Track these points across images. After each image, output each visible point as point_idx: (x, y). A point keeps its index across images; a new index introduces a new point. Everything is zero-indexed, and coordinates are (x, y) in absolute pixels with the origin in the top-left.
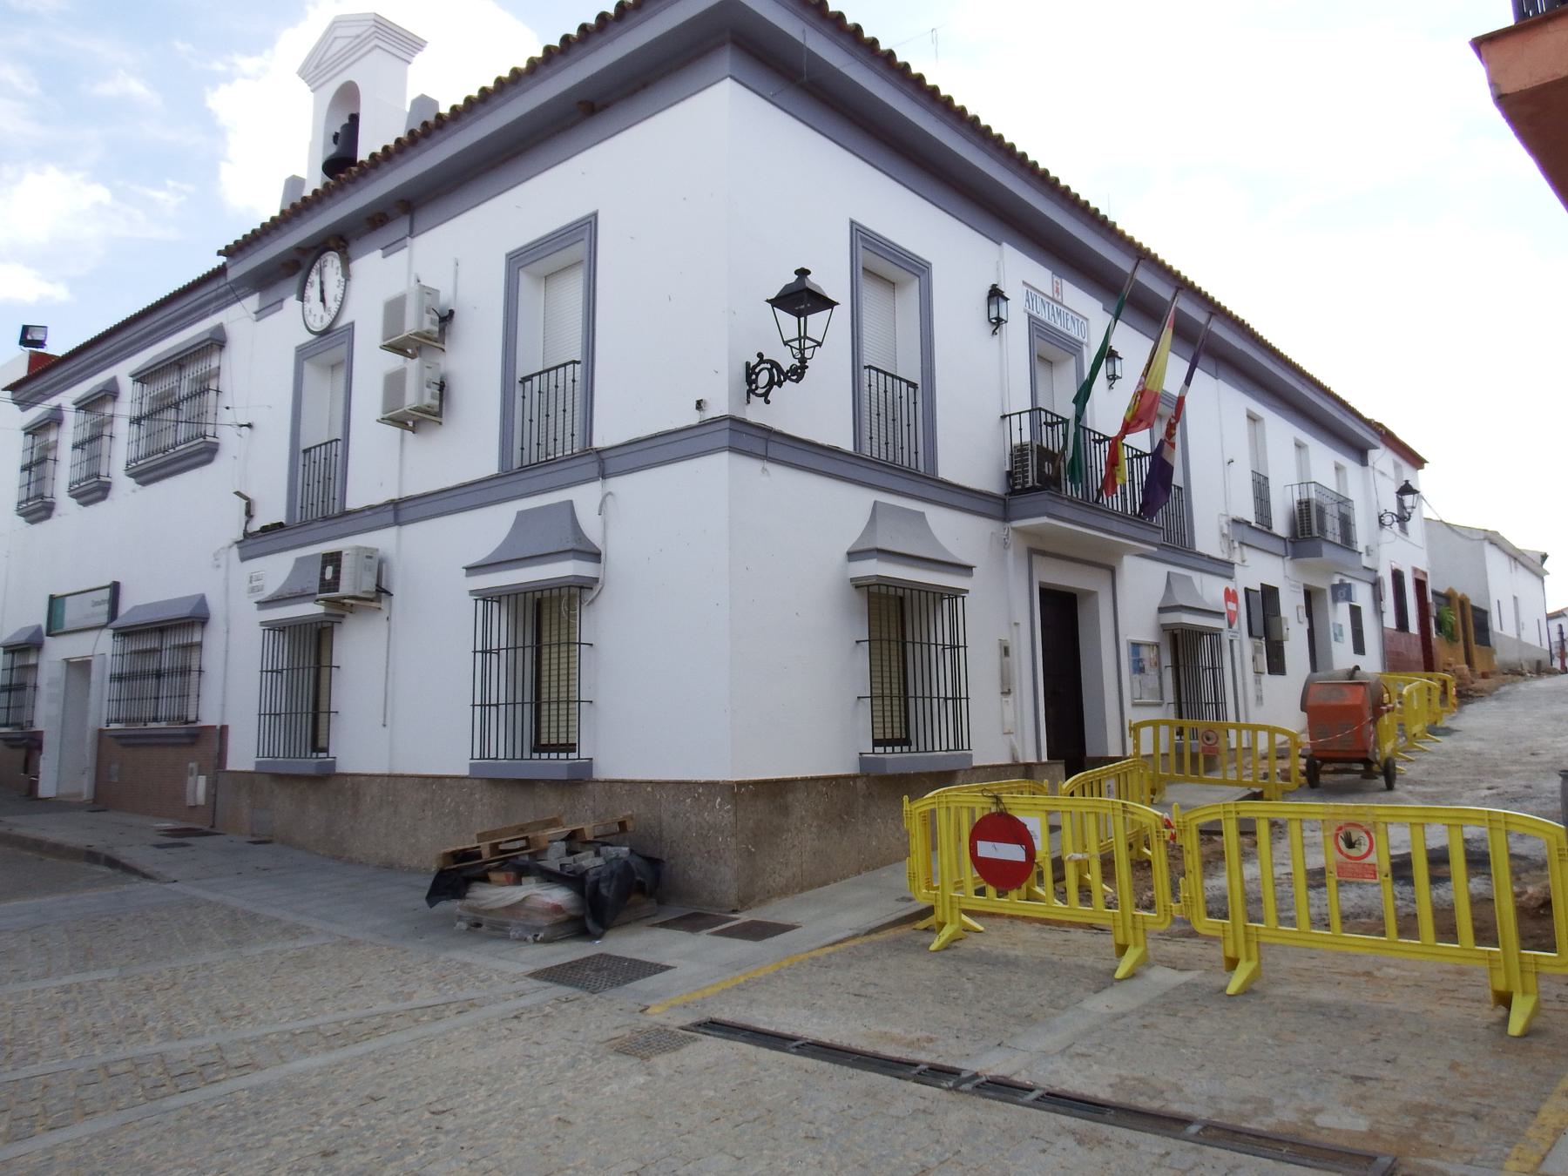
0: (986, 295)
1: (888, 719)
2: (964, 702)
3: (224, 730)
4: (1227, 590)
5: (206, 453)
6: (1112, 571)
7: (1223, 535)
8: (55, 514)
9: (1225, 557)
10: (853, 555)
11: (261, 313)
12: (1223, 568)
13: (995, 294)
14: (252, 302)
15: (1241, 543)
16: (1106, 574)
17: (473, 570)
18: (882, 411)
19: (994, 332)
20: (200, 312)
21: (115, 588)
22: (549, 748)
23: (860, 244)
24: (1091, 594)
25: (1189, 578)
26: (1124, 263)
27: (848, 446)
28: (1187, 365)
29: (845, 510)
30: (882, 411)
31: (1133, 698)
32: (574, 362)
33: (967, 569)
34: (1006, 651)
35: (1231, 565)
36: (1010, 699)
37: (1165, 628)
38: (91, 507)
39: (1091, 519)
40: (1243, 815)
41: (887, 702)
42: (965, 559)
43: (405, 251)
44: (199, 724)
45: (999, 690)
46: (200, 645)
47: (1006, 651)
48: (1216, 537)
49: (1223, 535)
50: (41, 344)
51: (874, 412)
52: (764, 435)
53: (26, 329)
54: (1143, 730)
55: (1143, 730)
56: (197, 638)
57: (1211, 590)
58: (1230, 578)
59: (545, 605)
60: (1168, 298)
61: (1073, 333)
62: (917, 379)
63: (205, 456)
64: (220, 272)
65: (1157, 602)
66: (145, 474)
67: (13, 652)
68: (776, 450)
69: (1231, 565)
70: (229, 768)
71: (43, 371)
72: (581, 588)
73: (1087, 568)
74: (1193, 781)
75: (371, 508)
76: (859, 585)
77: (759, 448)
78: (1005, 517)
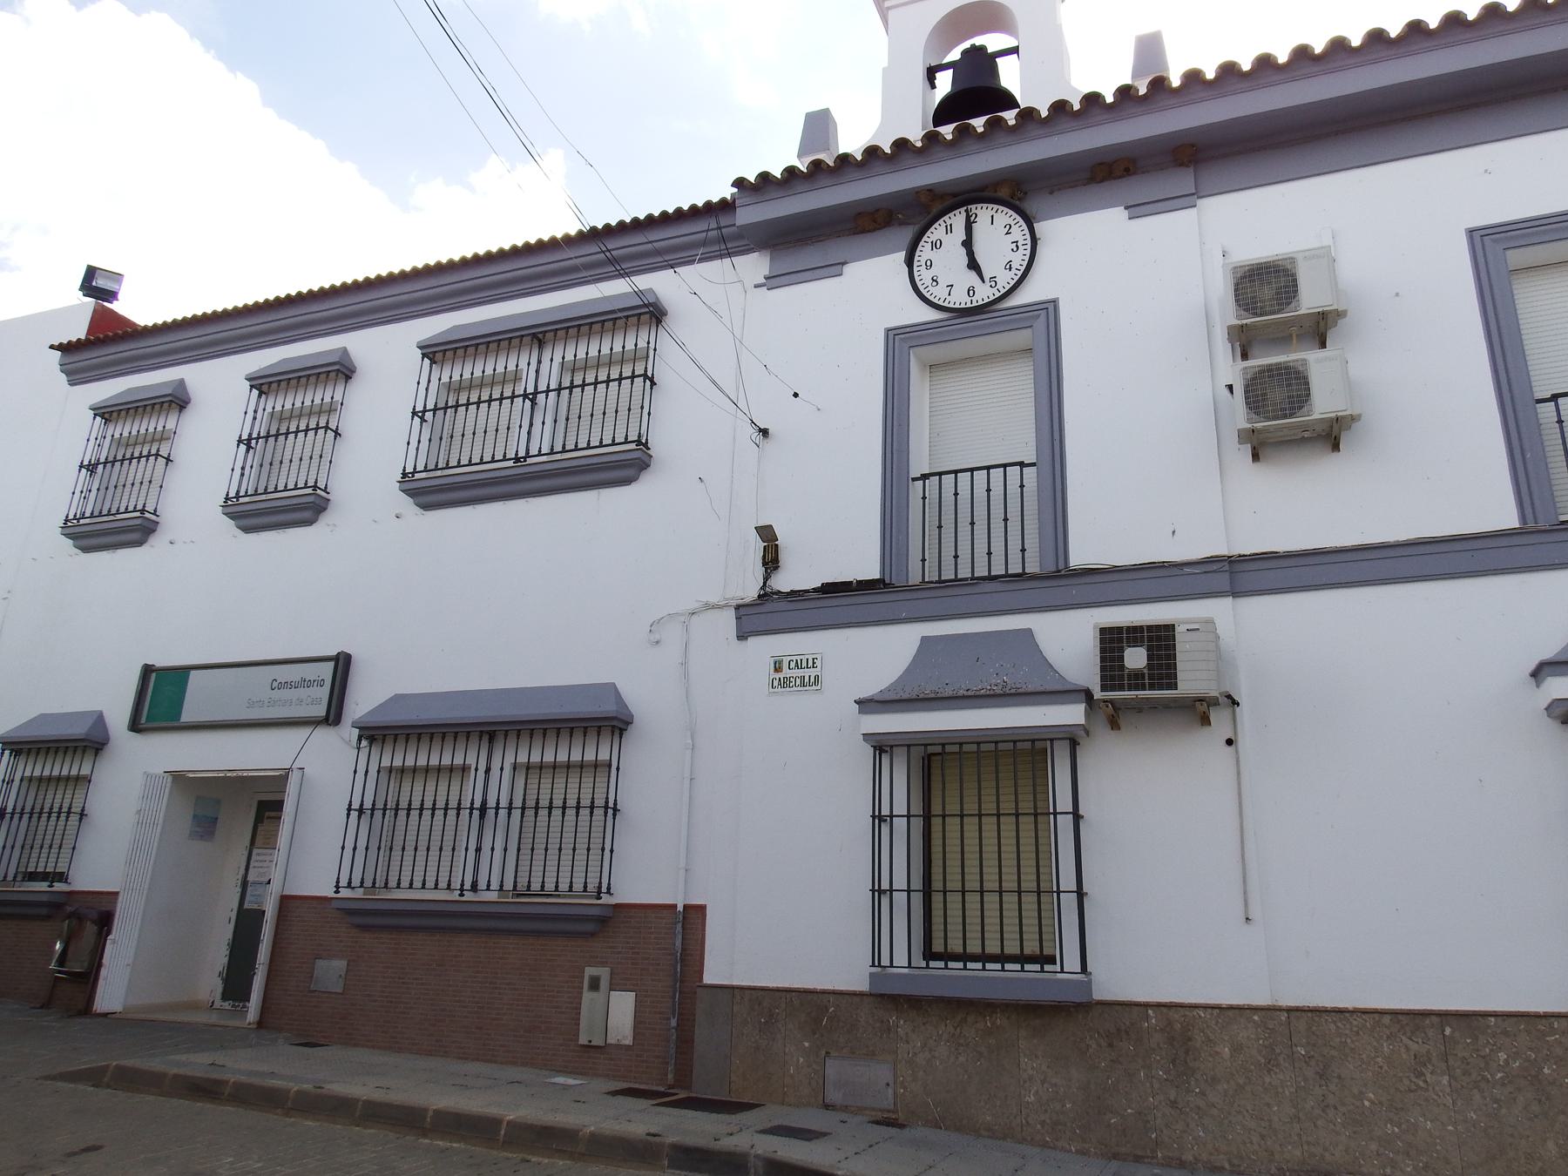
3: (694, 915)
5: (627, 465)
8: (325, 519)
11: (773, 281)
14: (755, 265)
17: (867, 705)
20: (618, 267)
21: (342, 664)
22: (947, 957)
32: (1022, 465)
38: (253, 537)
43: (1192, 211)
44: (605, 899)
46: (88, 780)
50: (111, 295)
53: (91, 272)
56: (85, 771)
59: (936, 762)
63: (307, 515)
64: (725, 206)
66: (432, 490)
67: (372, 740)
70: (708, 979)
71: (105, 341)
72: (1052, 740)
75: (1163, 565)
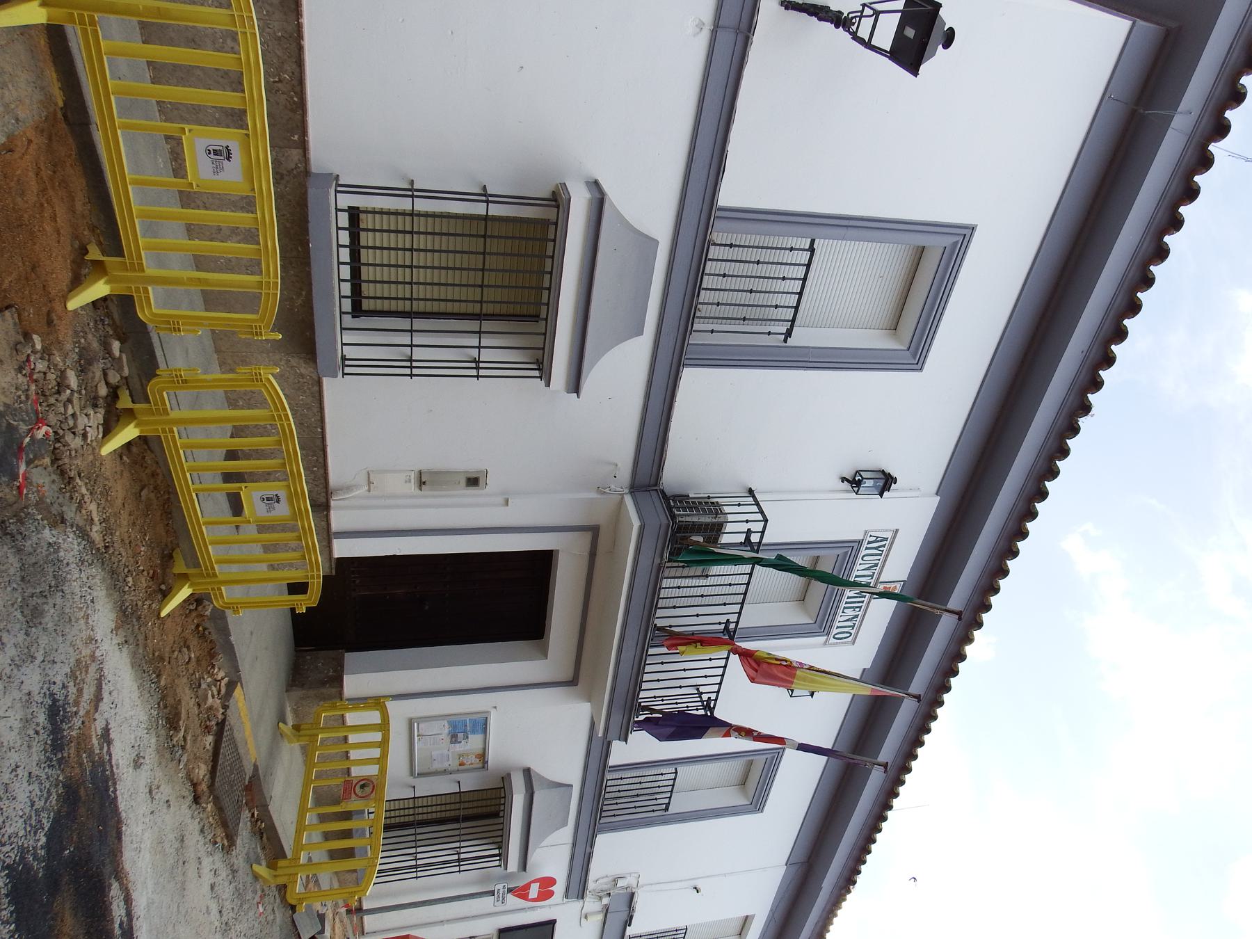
0: (888, 470)
1: (402, 812)
2: (414, 875)
4: (552, 881)
6: (572, 682)
7: (615, 881)
9: (591, 885)
10: (527, 772)
12: (578, 887)
13: (886, 482)
15: (606, 910)
16: (567, 674)
18: (644, 785)
19: (843, 479)
23: (769, 756)
24: (544, 654)
25: (565, 824)
26: (959, 598)
27: (613, 761)
28: (828, 744)
29: (648, 201)
30: (644, 785)
31: (421, 719)
33: (575, 386)
34: (473, 482)
35: (581, 895)
36: (412, 488)
37: (506, 779)
39: (630, 643)
40: (69, 29)
41: (411, 811)
42: (586, 386)
45: (424, 466)
47: (473, 482)
48: (615, 871)
49: (615, 881)
51: (643, 779)
52: (744, 26)
54: (377, 714)
55: (377, 714)
57: (551, 857)
58: (566, 896)
60: (912, 690)
61: (840, 620)
62: (672, 810)
65: (538, 768)
68: (726, 38)
69: (581, 895)
73: (578, 620)
74: (308, 773)
76: (558, 200)
77: (730, 18)
78: (635, 488)
